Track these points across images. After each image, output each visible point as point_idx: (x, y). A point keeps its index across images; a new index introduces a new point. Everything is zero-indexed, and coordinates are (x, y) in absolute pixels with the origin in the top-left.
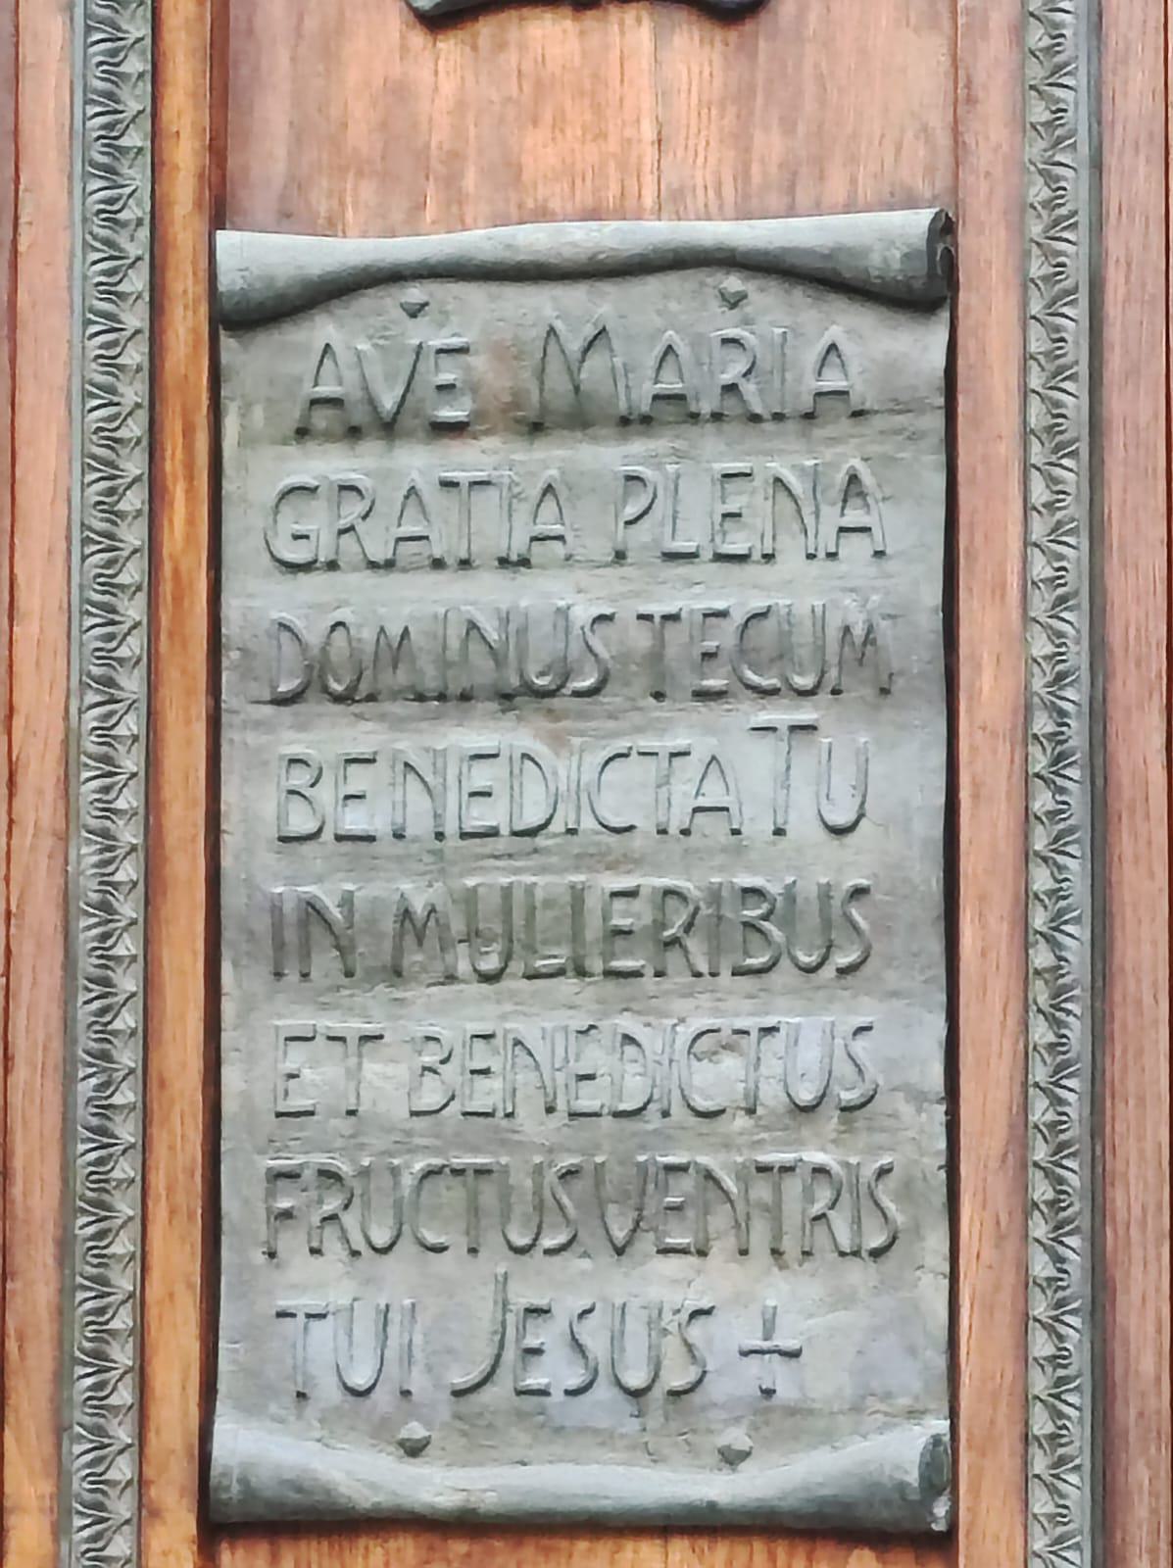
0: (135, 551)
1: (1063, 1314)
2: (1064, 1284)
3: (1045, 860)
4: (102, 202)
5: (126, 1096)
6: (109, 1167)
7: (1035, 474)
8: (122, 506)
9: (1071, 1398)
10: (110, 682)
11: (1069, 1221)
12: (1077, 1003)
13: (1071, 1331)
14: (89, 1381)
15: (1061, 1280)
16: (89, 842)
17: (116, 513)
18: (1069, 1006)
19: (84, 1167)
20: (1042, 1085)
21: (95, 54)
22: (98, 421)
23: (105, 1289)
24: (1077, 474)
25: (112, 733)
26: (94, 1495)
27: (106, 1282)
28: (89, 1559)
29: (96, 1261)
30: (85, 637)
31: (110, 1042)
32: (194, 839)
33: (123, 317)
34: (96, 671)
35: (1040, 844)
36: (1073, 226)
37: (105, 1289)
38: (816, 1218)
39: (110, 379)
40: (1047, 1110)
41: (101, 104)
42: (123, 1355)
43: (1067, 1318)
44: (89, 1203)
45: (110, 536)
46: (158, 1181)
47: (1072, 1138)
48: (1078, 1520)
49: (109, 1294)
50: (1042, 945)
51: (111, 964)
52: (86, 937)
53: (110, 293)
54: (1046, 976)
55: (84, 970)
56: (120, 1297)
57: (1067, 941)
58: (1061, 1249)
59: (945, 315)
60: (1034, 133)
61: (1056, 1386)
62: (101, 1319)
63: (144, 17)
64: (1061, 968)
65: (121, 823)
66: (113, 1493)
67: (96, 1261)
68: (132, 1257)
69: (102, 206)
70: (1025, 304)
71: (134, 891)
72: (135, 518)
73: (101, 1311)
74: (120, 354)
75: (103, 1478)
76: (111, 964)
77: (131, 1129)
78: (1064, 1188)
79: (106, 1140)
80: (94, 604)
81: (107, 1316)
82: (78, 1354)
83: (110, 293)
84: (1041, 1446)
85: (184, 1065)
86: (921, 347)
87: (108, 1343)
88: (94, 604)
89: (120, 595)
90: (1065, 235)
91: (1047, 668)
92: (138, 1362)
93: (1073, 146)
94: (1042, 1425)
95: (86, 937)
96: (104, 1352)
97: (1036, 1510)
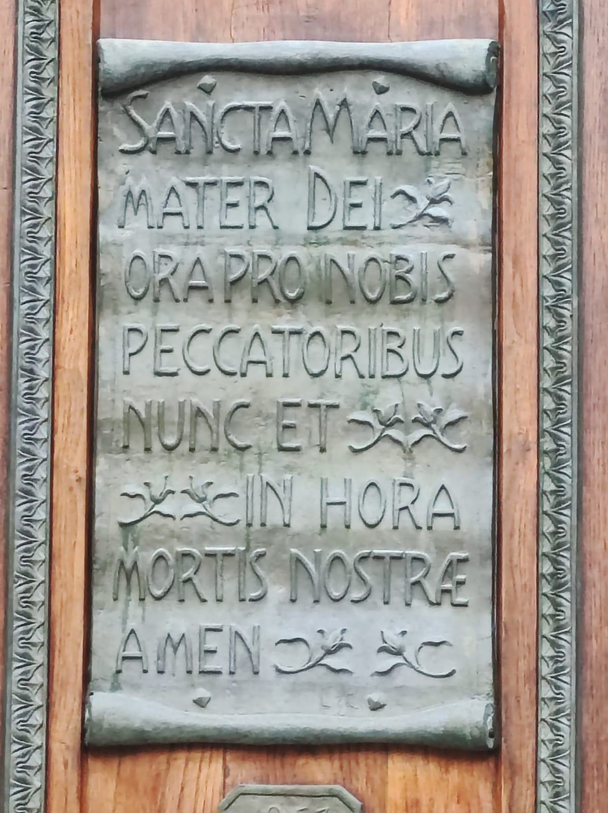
0: (38, 748)
1: (559, 675)
2: (562, 175)
3: (551, 434)
4: (33, 28)
5: (45, 232)
6: (31, 555)
7: (543, 683)
8: (36, 476)
9: (567, 234)
10: (33, 290)
11: (563, 668)
12: (566, 759)
13: (566, 118)
14: (21, 629)
15: (559, 615)
16: (22, 376)
17: (32, 480)
18: (565, 347)
19: (16, 677)
20: (548, 74)
21: (24, 267)
22: (24, 429)
23: (30, 620)
24: (571, 436)
25: (35, 317)
26: (30, 283)
27: (34, 413)
28: (19, 809)
29: (25, 605)
30: (24, 146)
31: (32, 485)
32: (78, 356)
33: (44, 92)
34: (27, 284)
35: (547, 507)
36: (570, 66)
37: (30, 620)
38: (414, 584)
39: (37, 125)
40: (549, 608)
41: (26, 335)
42: (41, 493)
43: (562, 636)
44: (24, 410)
45: (36, 211)
46: (55, 747)
47: (567, 623)
48: (570, 328)
49: (36, 459)
50: (548, 438)
51: (34, 402)
52: (24, 148)
53: (32, 318)
54: (550, 454)
55: (13, 774)
56: (37, 625)
57: (563, 643)
58: (560, 352)
59: (492, 99)
60: (545, 17)
61: (555, 630)
62: (34, 271)
63: (49, 329)
64: (559, 450)
65: (33, 733)
66: (33, 731)
67: (25, 605)
68: (50, 239)
69: (29, 230)
70: (539, 504)
71: (48, 325)
72: (41, 646)
73: (27, 632)
74: (36, 313)
75: (38, 195)
76: (34, 402)
77: (51, 131)
78: (562, 443)
79: (38, 215)
80: (30, 89)
81: (34, 431)
82: (17, 491)
83: (32, 318)
84: (545, 744)
85: (71, 598)
86: (480, 114)
87: (30, 649)
88: (30, 89)
89: (31, 689)
90: (565, 71)
91: (551, 663)
92: (52, 296)
93: (571, 25)
94: (548, 526)
95: (24, 148)
96: (35, 289)
97: (545, 294)
